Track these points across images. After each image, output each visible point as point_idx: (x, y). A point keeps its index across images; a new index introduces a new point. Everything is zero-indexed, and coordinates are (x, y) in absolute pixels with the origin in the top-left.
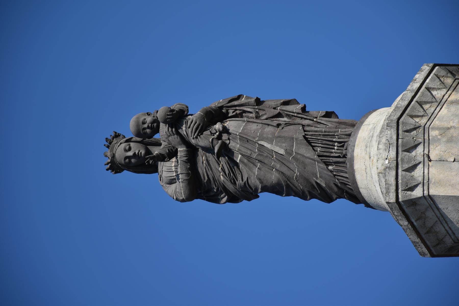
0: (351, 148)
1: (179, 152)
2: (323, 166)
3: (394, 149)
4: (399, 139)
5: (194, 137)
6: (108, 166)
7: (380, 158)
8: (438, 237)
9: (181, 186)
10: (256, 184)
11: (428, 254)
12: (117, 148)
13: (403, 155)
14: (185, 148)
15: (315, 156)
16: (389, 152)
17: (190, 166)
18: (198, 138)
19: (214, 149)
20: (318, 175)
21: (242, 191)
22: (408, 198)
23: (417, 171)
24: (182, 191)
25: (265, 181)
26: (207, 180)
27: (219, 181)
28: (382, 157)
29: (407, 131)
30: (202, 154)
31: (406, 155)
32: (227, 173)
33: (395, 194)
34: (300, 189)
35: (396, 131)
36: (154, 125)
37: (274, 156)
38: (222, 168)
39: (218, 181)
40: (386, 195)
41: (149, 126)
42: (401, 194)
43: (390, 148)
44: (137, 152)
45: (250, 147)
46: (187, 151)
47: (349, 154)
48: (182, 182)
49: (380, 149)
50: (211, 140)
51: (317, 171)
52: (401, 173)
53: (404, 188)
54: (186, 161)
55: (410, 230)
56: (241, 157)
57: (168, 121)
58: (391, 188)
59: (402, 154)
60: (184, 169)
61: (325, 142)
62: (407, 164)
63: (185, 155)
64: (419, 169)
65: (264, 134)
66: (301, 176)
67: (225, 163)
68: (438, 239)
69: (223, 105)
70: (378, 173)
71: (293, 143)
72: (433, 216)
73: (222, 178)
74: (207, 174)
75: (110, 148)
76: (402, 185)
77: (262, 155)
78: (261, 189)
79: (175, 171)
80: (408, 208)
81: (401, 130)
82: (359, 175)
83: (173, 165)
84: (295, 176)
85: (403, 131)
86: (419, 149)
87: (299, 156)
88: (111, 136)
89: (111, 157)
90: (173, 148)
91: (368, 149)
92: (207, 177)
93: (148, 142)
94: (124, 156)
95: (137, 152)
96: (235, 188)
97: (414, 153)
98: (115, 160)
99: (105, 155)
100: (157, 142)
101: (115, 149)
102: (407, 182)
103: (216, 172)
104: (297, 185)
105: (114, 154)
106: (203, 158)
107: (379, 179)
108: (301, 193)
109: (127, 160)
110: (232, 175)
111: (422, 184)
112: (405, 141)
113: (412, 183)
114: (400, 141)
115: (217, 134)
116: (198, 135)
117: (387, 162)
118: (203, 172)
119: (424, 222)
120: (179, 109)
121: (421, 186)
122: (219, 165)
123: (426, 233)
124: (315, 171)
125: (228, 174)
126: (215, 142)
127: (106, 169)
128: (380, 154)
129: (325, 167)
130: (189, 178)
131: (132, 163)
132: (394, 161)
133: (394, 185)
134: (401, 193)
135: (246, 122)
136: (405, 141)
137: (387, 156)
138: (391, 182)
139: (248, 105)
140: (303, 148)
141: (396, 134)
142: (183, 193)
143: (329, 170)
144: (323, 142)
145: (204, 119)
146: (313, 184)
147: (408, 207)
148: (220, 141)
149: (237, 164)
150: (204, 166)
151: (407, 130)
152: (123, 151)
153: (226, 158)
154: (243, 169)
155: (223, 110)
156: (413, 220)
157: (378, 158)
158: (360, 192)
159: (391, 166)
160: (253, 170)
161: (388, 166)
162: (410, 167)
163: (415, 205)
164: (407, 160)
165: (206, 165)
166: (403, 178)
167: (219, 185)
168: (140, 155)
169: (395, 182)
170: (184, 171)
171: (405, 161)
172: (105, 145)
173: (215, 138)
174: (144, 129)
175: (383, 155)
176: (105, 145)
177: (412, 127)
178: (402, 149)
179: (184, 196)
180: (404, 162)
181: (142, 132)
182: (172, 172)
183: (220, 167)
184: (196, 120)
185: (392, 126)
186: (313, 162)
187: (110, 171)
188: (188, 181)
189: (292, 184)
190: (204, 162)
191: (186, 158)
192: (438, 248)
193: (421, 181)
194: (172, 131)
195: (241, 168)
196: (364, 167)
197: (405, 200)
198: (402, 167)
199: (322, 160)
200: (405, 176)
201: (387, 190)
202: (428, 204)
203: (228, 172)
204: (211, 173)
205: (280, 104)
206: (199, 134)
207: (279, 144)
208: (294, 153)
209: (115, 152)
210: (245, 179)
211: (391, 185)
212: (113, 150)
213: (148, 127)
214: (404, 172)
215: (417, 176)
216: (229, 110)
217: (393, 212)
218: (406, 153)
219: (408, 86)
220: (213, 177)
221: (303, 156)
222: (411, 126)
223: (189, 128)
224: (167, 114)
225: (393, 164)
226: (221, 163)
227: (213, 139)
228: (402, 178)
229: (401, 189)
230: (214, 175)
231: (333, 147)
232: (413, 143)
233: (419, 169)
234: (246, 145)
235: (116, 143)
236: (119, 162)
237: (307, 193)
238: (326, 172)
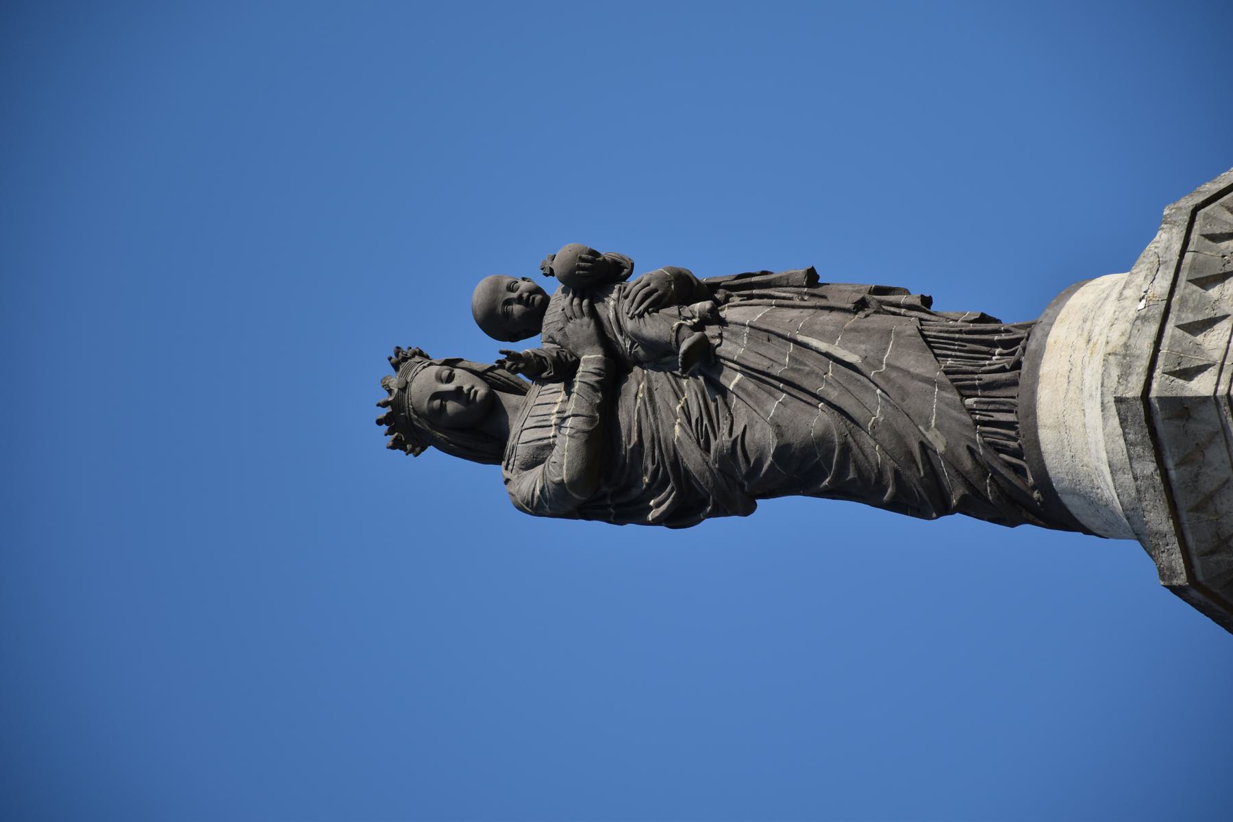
0: (1043, 330)
1: (582, 364)
2: (952, 396)
3: (1170, 273)
4: (1186, 254)
5: (637, 312)
6: (383, 412)
7: (1120, 319)
8: (1219, 529)
9: (566, 446)
10: (763, 441)
11: (1182, 573)
12: (418, 370)
13: (1187, 291)
14: (600, 356)
15: (938, 373)
16: (1152, 282)
17: (601, 401)
18: (644, 317)
19: (678, 347)
20: (933, 422)
21: (720, 470)
22: (1174, 394)
23: (1214, 336)
24: (565, 461)
25: (790, 431)
26: (634, 446)
27: (667, 441)
28: (1125, 316)
29: (1215, 238)
30: (640, 377)
31: (1194, 291)
32: (695, 414)
33: (1143, 378)
34: (874, 464)
35: (1184, 232)
36: (534, 299)
37: (830, 374)
38: (682, 407)
39: (665, 441)
40: (1120, 381)
41: (523, 298)
42: (1158, 381)
43: (1159, 272)
44: (466, 388)
45: (771, 354)
46: (606, 362)
47: (1034, 341)
48: (571, 436)
49: (1125, 298)
50: (676, 324)
51: (932, 411)
52: (1171, 331)
53: (1170, 368)
54: (596, 385)
55: (1155, 491)
56: (741, 379)
57: (579, 274)
58: (1138, 363)
59: (1185, 288)
60: (585, 404)
61: (970, 346)
62: (1191, 312)
63: (597, 371)
64: (1218, 332)
65: (816, 324)
66: (887, 425)
67: (696, 394)
68: (1218, 535)
69: (721, 282)
70: (1105, 355)
71: (888, 343)
72: (1223, 462)
73: (677, 432)
74: (638, 428)
75: (401, 369)
76: (1167, 359)
77: (800, 370)
78: (774, 456)
79: (555, 425)
80: (1167, 421)
81: (1198, 233)
82: (1047, 391)
83: (560, 399)
84: (872, 420)
85: (1203, 235)
86: (1230, 286)
87: (894, 375)
88: (410, 348)
89: (399, 389)
90: (568, 356)
91: (1089, 323)
92: (638, 437)
93: (499, 380)
94: (433, 391)
95: (466, 388)
96: (704, 459)
97: (1214, 292)
98: (406, 398)
99: (385, 382)
100: (521, 386)
101: (412, 372)
102: (1182, 355)
103: (666, 415)
104: (868, 451)
105: (407, 383)
106: (639, 384)
107: (1104, 371)
108: (873, 475)
109: (437, 403)
110: (705, 422)
111: (1219, 367)
112: (1200, 258)
113: (1193, 360)
114: (1188, 257)
115: (695, 320)
116: (646, 310)
117: (1142, 305)
118: (630, 422)
119: (1197, 475)
120: (612, 259)
121: (1213, 371)
122: (678, 398)
123: (1191, 510)
124: (929, 410)
125: (697, 420)
126: (685, 331)
127: (375, 420)
128: (1124, 309)
129: (958, 398)
130: (591, 429)
131: (447, 414)
132: (1160, 303)
133: (1147, 356)
134: (1161, 378)
135: (774, 307)
136: (1200, 258)
137: (1146, 292)
138: (1140, 351)
139: (785, 282)
140: (909, 355)
141: (1183, 239)
142: (564, 467)
143: (964, 406)
144: (966, 346)
145: (670, 285)
146: (911, 452)
147: (1169, 419)
148: (697, 334)
149: (723, 391)
150: (638, 405)
151: (1212, 234)
152: (434, 378)
153: (701, 378)
154: (740, 408)
155: (715, 295)
156: (1170, 463)
157: (1116, 319)
158: (1040, 447)
159: (1150, 313)
160: (766, 405)
161: (1143, 313)
162: (1198, 321)
163: (1187, 420)
164: (1196, 303)
165: (642, 403)
166: (1173, 343)
167: (664, 452)
168: (472, 395)
169: (1152, 350)
170: (584, 410)
171: (1189, 305)
172: (390, 359)
173: (687, 326)
174: (508, 302)
175: (1130, 312)
176: (390, 359)
177: (1227, 231)
178: (1188, 276)
179: (567, 475)
180: (1186, 307)
181: (500, 310)
182: (547, 428)
183: (680, 403)
184: (650, 279)
185: (1175, 222)
186: (929, 387)
187: (385, 428)
188: (586, 435)
189: (857, 444)
190: (641, 395)
191: (598, 378)
192: (1211, 559)
193: (1217, 359)
194: (580, 305)
195: (735, 406)
196: (1067, 368)
197: (1167, 397)
198: (1178, 318)
199: (953, 381)
200: (1179, 341)
201: (1125, 369)
202: (1219, 423)
203: (698, 415)
204: (652, 421)
205: (868, 290)
206: (650, 310)
207: (850, 345)
208: (884, 367)
209: (413, 378)
210: (738, 431)
211: (1138, 357)
212: (407, 374)
213: (520, 300)
214: (1181, 331)
215: (1210, 347)
216: (732, 296)
217: (1127, 430)
218: (1195, 287)
219: (1160, 472)
220: (653, 435)
221: (907, 373)
222: (1225, 227)
223: (626, 297)
224: (580, 257)
225: (1156, 309)
226: (684, 396)
227: (680, 326)
228: (1170, 343)
229: (1161, 367)
230: (657, 427)
231: (989, 356)
232: (1220, 267)
233: (1218, 332)
234: (762, 350)
235: (418, 363)
236: (415, 406)
237: (889, 475)
238: (954, 413)
